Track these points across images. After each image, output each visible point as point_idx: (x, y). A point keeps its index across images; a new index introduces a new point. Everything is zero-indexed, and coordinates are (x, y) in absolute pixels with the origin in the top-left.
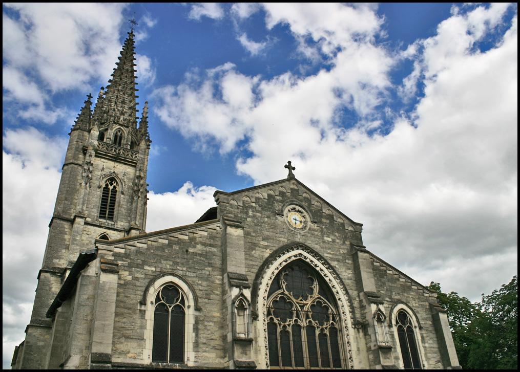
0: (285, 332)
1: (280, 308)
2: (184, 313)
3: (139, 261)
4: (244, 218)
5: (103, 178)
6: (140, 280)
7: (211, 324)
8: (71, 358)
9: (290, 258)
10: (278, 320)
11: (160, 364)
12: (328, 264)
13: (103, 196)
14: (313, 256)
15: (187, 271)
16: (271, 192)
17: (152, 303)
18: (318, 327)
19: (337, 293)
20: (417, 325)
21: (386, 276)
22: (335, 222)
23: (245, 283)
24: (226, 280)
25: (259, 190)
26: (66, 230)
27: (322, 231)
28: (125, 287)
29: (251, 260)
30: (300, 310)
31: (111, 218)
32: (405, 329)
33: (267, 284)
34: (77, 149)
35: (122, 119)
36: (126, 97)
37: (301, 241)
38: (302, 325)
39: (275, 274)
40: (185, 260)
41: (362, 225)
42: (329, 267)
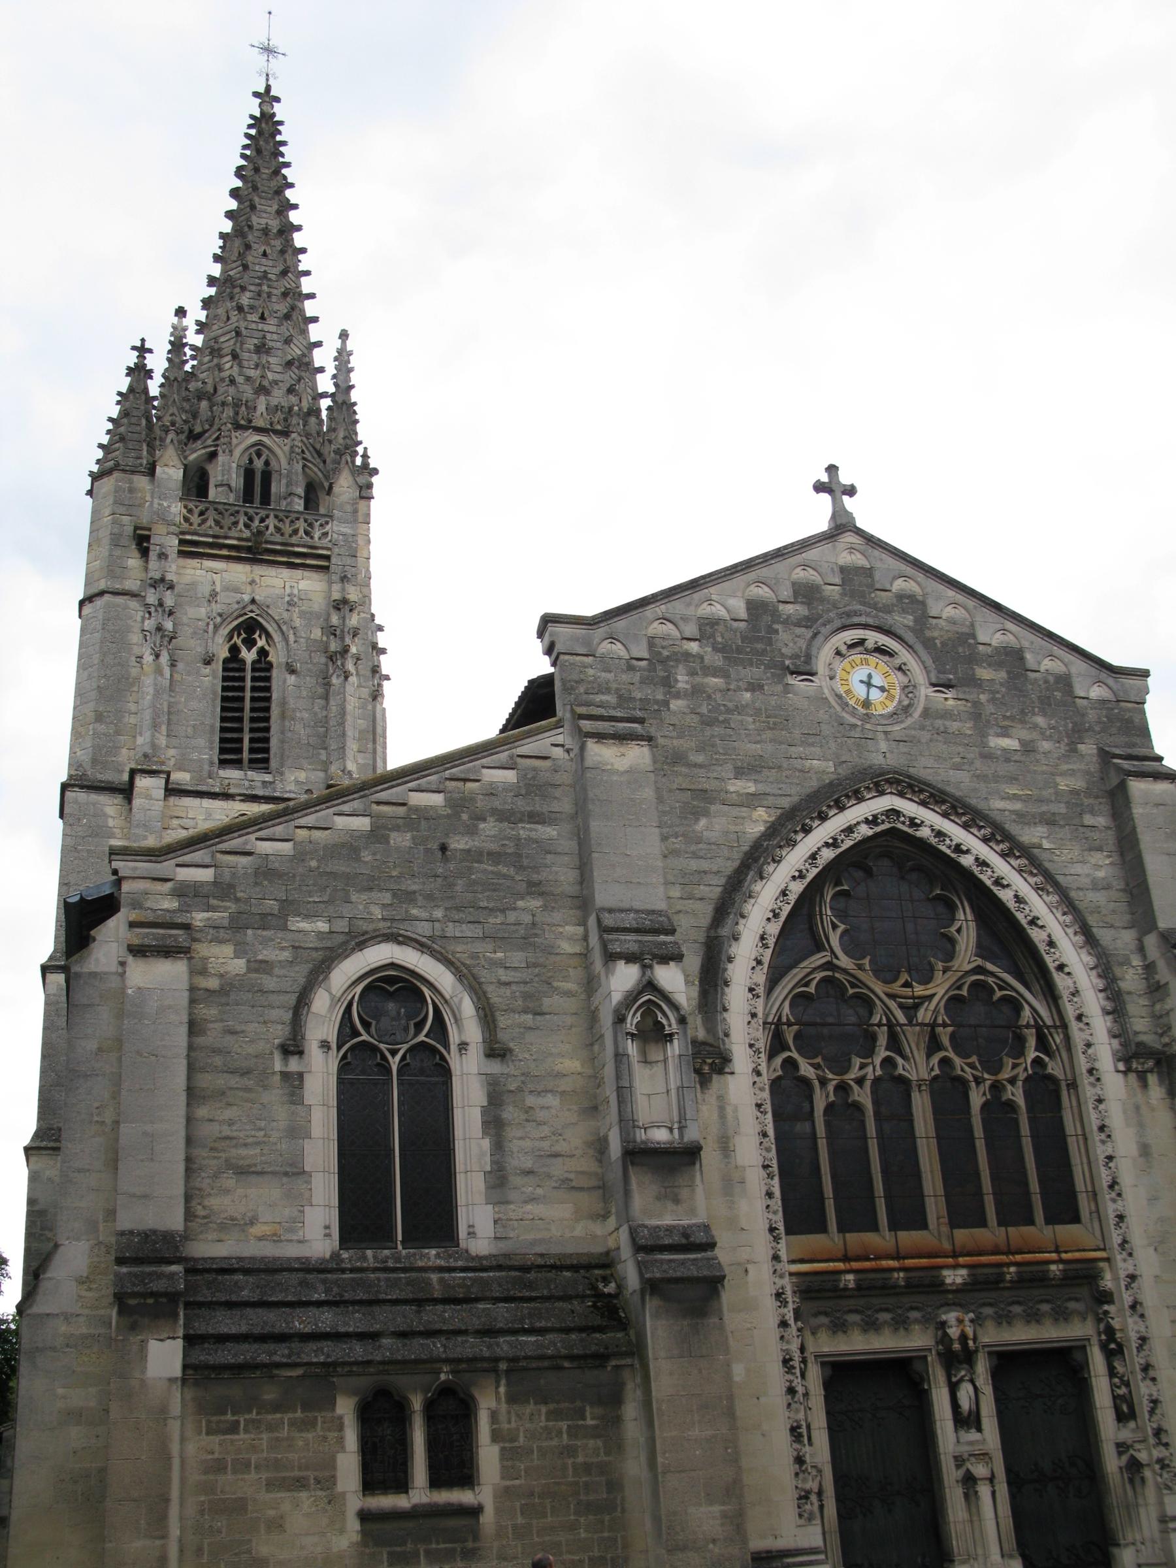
0: (843, 1109)
1: (819, 1025)
2: (445, 1071)
3: (271, 905)
4: (657, 702)
5: (216, 628)
6: (277, 971)
7: (552, 1101)
8: (61, 1249)
9: (849, 830)
10: (817, 1067)
11: (369, 1253)
12: (1007, 837)
13: (224, 689)
14: (945, 815)
15: (448, 919)
16: (763, 592)
18: (978, 1081)
19: (1051, 944)
22: (1032, 675)
24: (594, 940)
25: (712, 590)
26: (111, 823)
28: (223, 1000)
29: (695, 855)
30: (902, 1019)
31: (260, 759)
33: (762, 938)
34: (116, 541)
35: (261, 408)
36: (273, 329)
39: (793, 898)
40: (439, 880)
41: (1145, 674)
42: (1011, 849)
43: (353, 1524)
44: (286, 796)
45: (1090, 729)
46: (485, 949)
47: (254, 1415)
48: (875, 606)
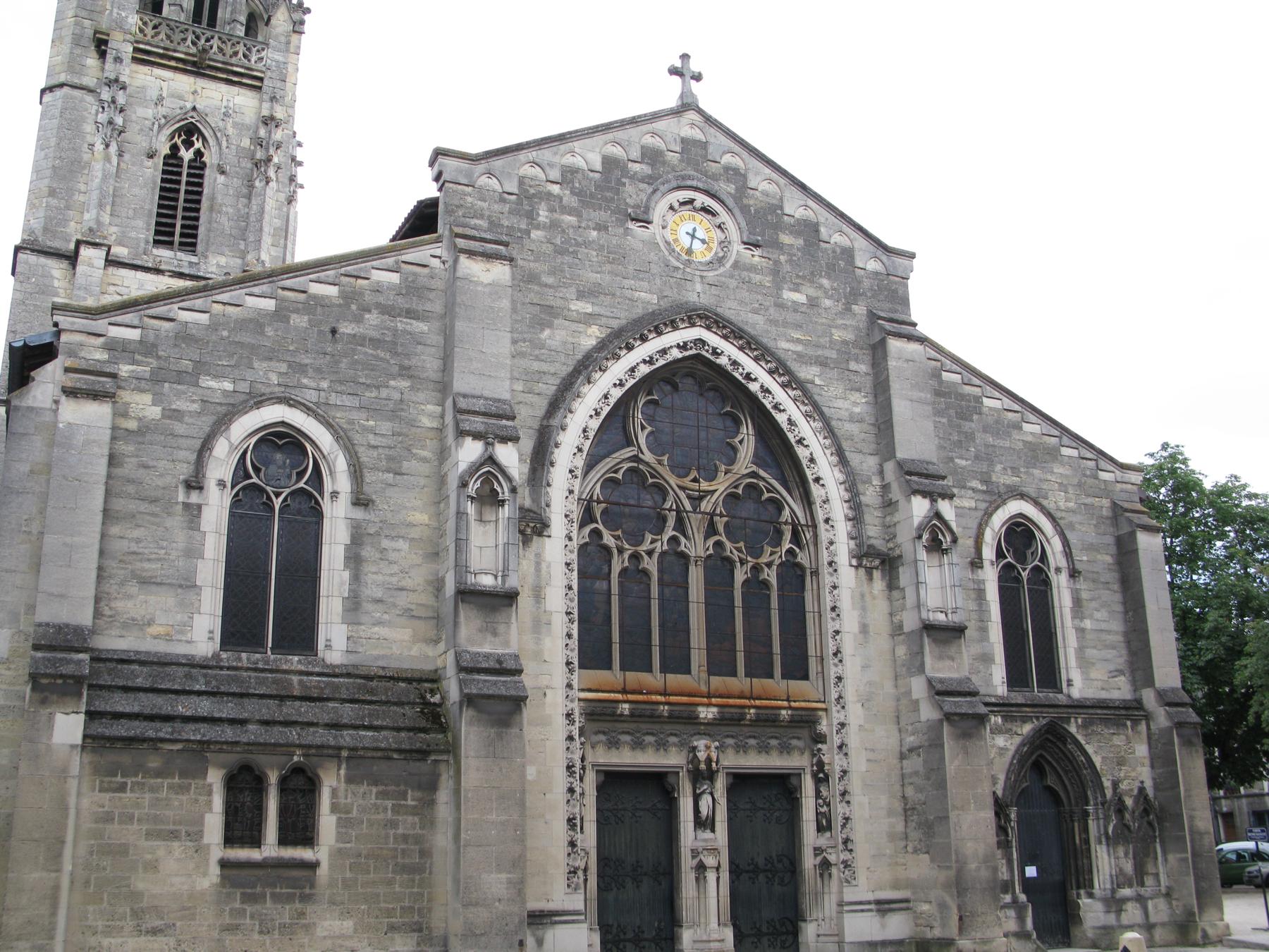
0: (635, 574)
3: (186, 365)
4: (520, 230)
5: (161, 127)
7: (402, 545)
9: (664, 352)
10: (617, 538)
14: (741, 348)
16: (617, 151)
17: (221, 484)
19: (812, 460)
20: (1063, 563)
26: (56, 283)
29: (537, 358)
32: (1025, 574)
39: (612, 401)
43: (215, 870)
45: (864, 294)
47: (139, 779)
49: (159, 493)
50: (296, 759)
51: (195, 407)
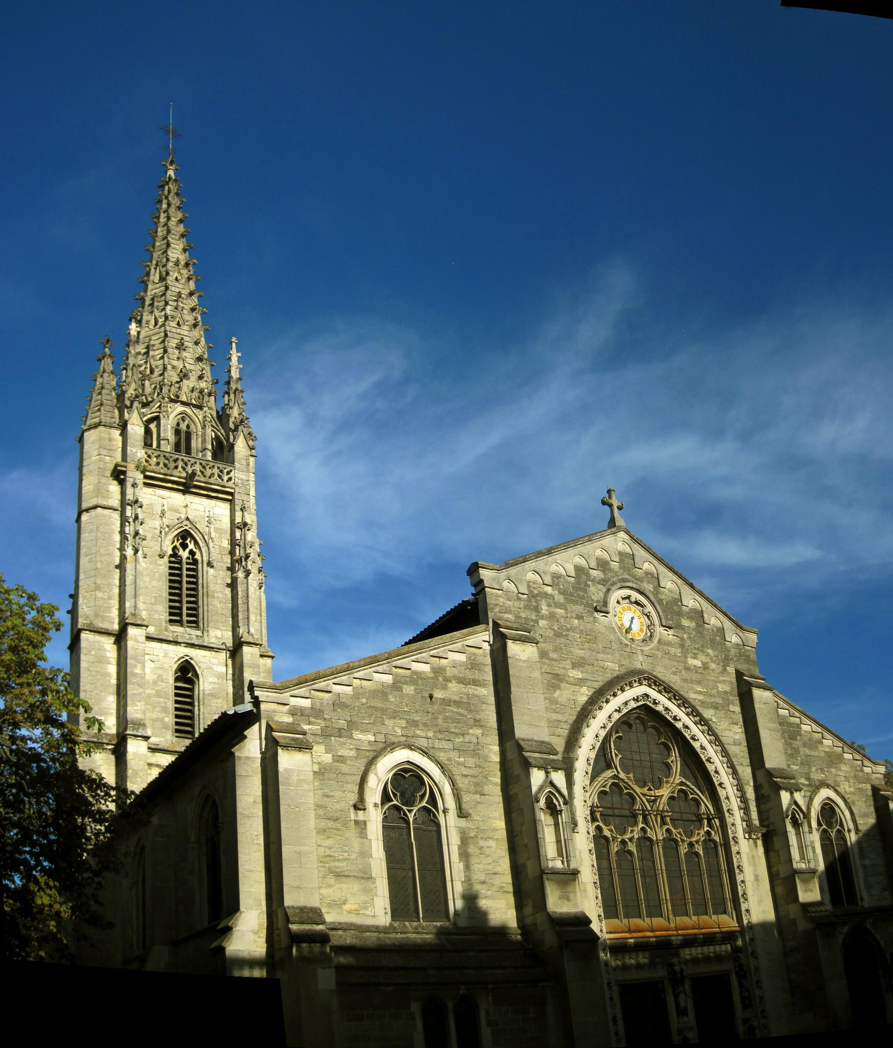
0: (624, 851)
1: (614, 808)
3: (342, 723)
4: (532, 620)
6: (348, 762)
7: (492, 843)
9: (626, 703)
10: (611, 830)
11: (407, 923)
12: (699, 714)
14: (669, 699)
16: (582, 562)
17: (376, 805)
19: (717, 772)
20: (851, 826)
21: (801, 735)
23: (553, 760)
26: (108, 655)
27: (682, 646)
28: (321, 777)
31: (195, 623)
35: (185, 389)
36: (186, 333)
37: (645, 667)
38: (655, 839)
44: (211, 645)
45: (732, 659)
46: (454, 755)
48: (634, 577)
49: (338, 814)
50: (462, 992)
51: (353, 753)
